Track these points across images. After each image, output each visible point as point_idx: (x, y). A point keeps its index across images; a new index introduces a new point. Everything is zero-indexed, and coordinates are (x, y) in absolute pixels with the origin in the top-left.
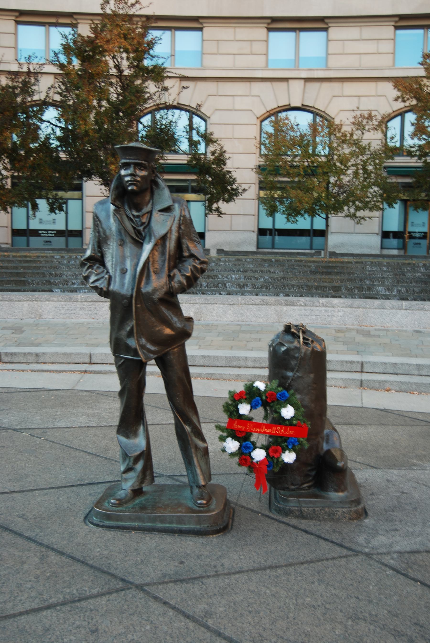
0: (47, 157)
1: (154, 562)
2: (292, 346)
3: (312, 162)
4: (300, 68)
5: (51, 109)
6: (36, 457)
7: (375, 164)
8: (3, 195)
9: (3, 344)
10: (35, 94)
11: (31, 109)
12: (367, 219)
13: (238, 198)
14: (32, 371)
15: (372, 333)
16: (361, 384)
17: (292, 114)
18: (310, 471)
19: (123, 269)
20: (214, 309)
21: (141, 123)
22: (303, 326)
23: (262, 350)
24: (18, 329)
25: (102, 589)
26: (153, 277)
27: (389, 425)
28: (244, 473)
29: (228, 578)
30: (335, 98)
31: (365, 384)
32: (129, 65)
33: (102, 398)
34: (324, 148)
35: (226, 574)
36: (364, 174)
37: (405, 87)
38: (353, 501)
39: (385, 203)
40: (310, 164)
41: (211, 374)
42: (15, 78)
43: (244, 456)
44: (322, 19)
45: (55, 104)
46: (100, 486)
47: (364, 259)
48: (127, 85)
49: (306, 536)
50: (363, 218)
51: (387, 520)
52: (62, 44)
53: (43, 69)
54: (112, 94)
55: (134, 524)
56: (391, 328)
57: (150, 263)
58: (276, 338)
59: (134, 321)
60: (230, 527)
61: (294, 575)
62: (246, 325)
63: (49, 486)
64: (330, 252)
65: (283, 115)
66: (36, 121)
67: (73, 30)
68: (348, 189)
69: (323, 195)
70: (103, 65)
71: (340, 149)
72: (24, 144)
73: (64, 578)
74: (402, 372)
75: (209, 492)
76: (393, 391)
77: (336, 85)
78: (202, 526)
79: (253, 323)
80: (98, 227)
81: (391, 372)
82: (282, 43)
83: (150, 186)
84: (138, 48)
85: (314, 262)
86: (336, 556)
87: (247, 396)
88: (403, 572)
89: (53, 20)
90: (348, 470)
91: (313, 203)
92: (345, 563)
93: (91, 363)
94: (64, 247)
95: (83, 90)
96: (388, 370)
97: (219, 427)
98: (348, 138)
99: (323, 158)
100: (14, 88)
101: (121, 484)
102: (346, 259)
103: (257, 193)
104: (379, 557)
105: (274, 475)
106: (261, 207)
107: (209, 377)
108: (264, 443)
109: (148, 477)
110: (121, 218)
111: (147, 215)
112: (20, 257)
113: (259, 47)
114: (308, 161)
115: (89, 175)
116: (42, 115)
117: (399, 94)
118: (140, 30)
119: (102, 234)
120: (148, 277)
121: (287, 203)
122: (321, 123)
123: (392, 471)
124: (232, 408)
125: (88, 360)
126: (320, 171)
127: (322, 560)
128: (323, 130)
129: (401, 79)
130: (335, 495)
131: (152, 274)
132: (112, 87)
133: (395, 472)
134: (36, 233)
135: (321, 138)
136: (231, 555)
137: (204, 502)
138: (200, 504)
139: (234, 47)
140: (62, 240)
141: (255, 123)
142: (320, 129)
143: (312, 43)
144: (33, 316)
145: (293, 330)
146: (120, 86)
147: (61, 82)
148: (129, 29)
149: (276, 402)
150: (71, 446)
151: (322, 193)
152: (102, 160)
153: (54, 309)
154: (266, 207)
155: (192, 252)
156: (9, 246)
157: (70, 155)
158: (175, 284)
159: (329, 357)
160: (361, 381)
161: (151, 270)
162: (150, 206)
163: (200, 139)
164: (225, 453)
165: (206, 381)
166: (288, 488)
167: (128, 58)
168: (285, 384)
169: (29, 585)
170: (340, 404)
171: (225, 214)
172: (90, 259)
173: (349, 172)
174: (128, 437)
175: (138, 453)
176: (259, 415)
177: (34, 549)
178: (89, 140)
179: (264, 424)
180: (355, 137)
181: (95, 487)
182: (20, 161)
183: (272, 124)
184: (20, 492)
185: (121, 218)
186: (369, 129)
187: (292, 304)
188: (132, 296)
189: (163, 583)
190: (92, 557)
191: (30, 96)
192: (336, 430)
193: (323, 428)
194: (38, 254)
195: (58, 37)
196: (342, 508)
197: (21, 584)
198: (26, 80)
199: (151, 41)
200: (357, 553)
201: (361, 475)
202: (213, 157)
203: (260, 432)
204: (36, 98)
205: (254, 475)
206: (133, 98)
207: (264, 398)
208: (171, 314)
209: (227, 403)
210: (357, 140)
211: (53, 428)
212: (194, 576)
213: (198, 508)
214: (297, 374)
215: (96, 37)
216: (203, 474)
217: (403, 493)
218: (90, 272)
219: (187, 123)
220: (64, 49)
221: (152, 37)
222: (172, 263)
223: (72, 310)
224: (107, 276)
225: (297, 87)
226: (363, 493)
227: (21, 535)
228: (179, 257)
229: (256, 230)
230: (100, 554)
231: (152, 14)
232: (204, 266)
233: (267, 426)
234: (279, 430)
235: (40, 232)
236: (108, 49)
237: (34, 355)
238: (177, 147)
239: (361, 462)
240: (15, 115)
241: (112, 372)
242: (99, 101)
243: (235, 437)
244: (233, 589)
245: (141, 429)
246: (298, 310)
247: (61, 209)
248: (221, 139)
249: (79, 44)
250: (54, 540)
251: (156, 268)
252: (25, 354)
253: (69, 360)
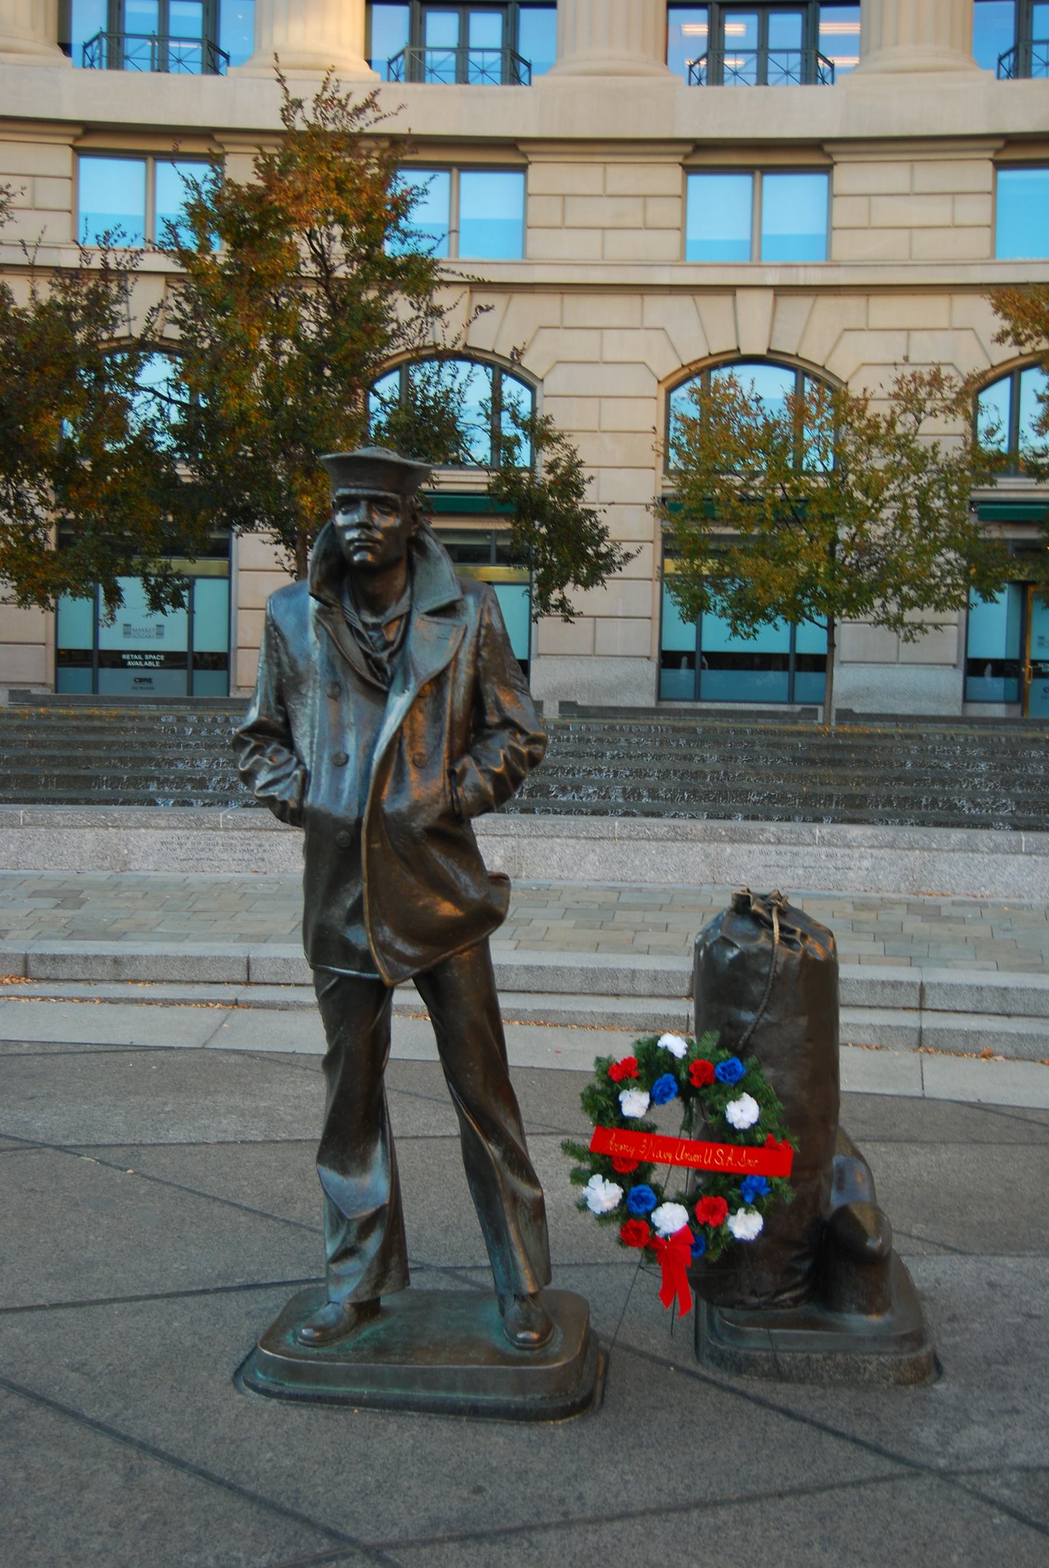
0: (145, 474)
1: (409, 1488)
2: (753, 947)
3: (795, 490)
4: (764, 262)
5: (158, 358)
6: (114, 1217)
7: (950, 496)
8: (37, 566)
9: (33, 933)
10: (120, 323)
11: (108, 360)
12: (930, 628)
13: (612, 575)
14: (103, 1000)
15: (944, 912)
16: (920, 1039)
17: (744, 374)
18: (799, 1259)
19: (337, 756)
20: (552, 850)
21: (376, 394)
22: (780, 898)
23: (673, 954)
24: (69, 897)
25: (280, 1556)
26: (413, 775)
27: (990, 1143)
28: (632, 1264)
29: (595, 1532)
30: (847, 333)
31: (929, 1040)
32: (347, 255)
33: (278, 1069)
34: (823, 457)
35: (590, 1521)
36: (921, 520)
37: (1022, 310)
38: (905, 1337)
39: (972, 590)
40: (791, 495)
41: (548, 1012)
42: (73, 285)
43: (632, 1222)
44: (816, 145)
45: (167, 348)
46: (272, 1292)
47: (923, 729)
48: (344, 302)
49: (790, 1424)
50: (920, 627)
51: (991, 1385)
52: (186, 205)
53: (140, 263)
54: (305, 324)
55: (357, 1390)
56: (991, 900)
57: (406, 742)
58: (713, 927)
59: (365, 885)
60: (598, 1399)
61: (762, 1524)
62: (631, 890)
63: (147, 1291)
64: (838, 710)
65: (722, 375)
66: (120, 390)
67: (214, 171)
68: (883, 555)
69: (821, 570)
70: (285, 253)
71: (862, 458)
72: (90, 447)
73: (183, 1526)
74: (1022, 1011)
75: (545, 1312)
76: (1000, 1058)
77: (853, 304)
78: (529, 1397)
79: (648, 885)
80: (277, 651)
81: (993, 1010)
82: (719, 205)
83: (407, 553)
84: (369, 214)
85: (800, 734)
86: (865, 1476)
87: (642, 1071)
88: (1034, 1519)
89: (166, 146)
91: (797, 590)
92: (888, 1496)
93: (248, 983)
94: (183, 695)
95: (236, 315)
96: (985, 1005)
97: (570, 1149)
98: (882, 431)
99: (820, 479)
100: (69, 308)
101: (326, 1289)
102: (878, 728)
103: (659, 563)
104: (974, 1479)
105: (704, 1269)
106: (667, 597)
107: (543, 1019)
108: (682, 1189)
109: (393, 1272)
110: (335, 630)
111: (397, 623)
112: (76, 717)
113: (665, 212)
114: (783, 488)
115: (247, 519)
116: (135, 374)
117: (1007, 325)
118: (376, 170)
119: (287, 669)
120: (400, 775)
121: (731, 589)
122: (816, 396)
123: (1000, 1260)
124: (603, 1101)
125: (241, 976)
126: (813, 510)
127: (831, 1487)
128: (820, 413)
129: (1013, 289)
130: (861, 1323)
131: (410, 767)
132: (307, 308)
133: (1010, 1262)
134: (115, 659)
135: (816, 432)
136: (602, 1472)
137: (534, 1336)
138: (524, 1341)
139: (602, 212)
140: (178, 677)
141: (654, 394)
142: (814, 410)
143: (793, 203)
144: (106, 864)
145: (754, 907)
146: (325, 305)
147: (181, 294)
148: (350, 168)
149: (713, 1086)
150: (201, 1190)
151: (818, 566)
152: (279, 485)
153: (159, 845)
154: (679, 599)
155: (509, 714)
156: (49, 692)
157: (202, 470)
158: (466, 794)
159: (845, 971)
160: (921, 1032)
161: (408, 758)
162: (405, 601)
163: (520, 432)
164: (583, 1214)
165: (533, 1029)
166: (742, 1302)
167: (345, 238)
168: (735, 1042)
169: (96, 1545)
170: (867, 1090)
171: (580, 614)
172: (256, 729)
173: (886, 513)
174: (344, 1171)
175: (370, 1211)
176: (671, 1118)
177: (110, 1451)
178: (248, 435)
179: (684, 1142)
180: (899, 429)
181: (261, 1295)
182: (79, 485)
183: (695, 396)
184: (73, 1305)
185: (335, 630)
186: (934, 410)
187: (747, 838)
188: (359, 822)
189: (432, 1541)
190: (253, 1473)
191: (106, 328)
192: (860, 1157)
193: (830, 1153)
194: (122, 712)
195: (175, 188)
196: (880, 1353)
197: (76, 1541)
198: (95, 289)
199: (402, 198)
200: (917, 1470)
201: (924, 1270)
202: (551, 477)
203: (674, 1162)
204: (120, 332)
205: (657, 1269)
206: (357, 334)
207: (683, 1075)
208: (455, 866)
209: (591, 1088)
210: (906, 436)
211: (154, 1145)
212: (510, 1525)
213: (518, 1353)
214: (766, 1016)
215: (270, 188)
216: (531, 1266)
217: (1030, 1316)
218: (256, 762)
219: (488, 394)
220: (190, 215)
221: (403, 187)
222: (458, 742)
223: (202, 850)
224: (297, 772)
225: (755, 309)
226: (929, 1316)
227: (76, 1415)
228: (475, 726)
229: (656, 654)
230: (274, 1466)
231: (405, 131)
232: (538, 749)
233: (692, 1147)
234: (721, 1157)
235: (124, 657)
236: (298, 217)
237: (108, 962)
238: (461, 451)
239: (923, 1235)
240: (71, 374)
241: (301, 1006)
242: (275, 341)
243: (611, 1175)
244: (607, 1560)
245: (378, 1151)
246: (761, 852)
247: (178, 603)
248: (571, 432)
249: (228, 203)
250: (159, 1430)
251: (420, 754)
252: (86, 958)
253: (194, 973)
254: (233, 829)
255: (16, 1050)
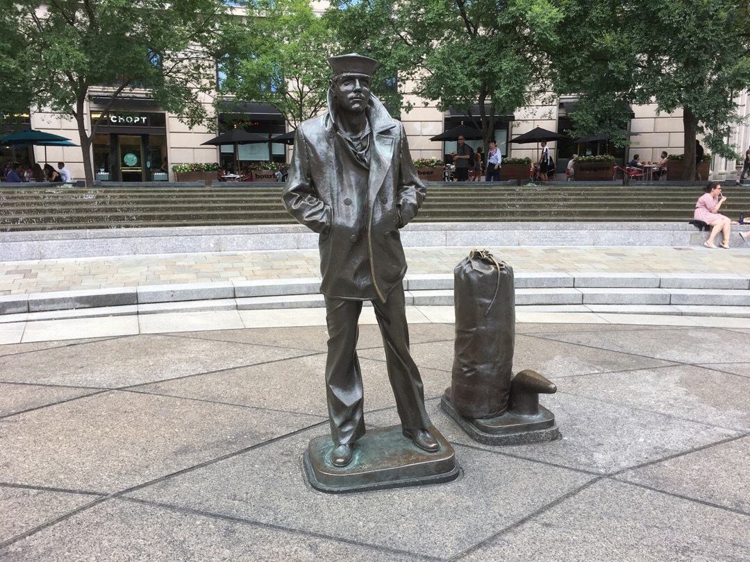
16: (237, 308)
20: (234, 239)
31: (417, 302)
90: (525, 372)
159: (516, 276)
254: (93, 238)
255: (51, 345)
